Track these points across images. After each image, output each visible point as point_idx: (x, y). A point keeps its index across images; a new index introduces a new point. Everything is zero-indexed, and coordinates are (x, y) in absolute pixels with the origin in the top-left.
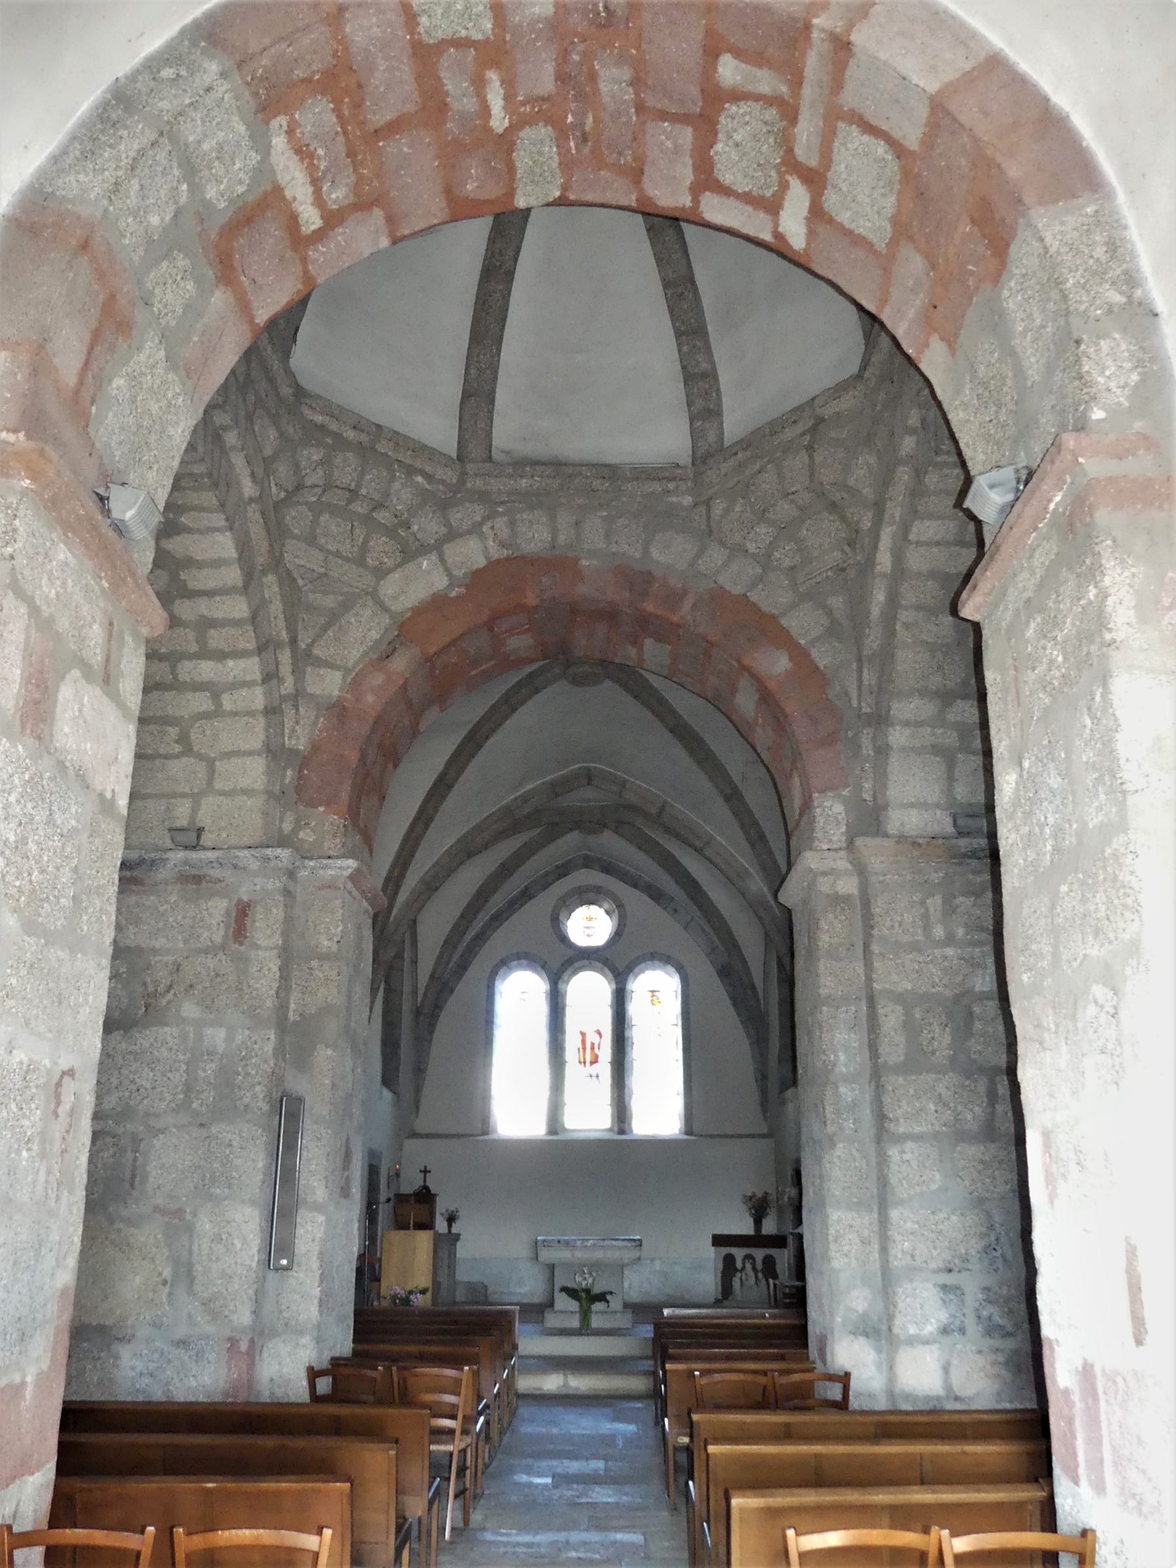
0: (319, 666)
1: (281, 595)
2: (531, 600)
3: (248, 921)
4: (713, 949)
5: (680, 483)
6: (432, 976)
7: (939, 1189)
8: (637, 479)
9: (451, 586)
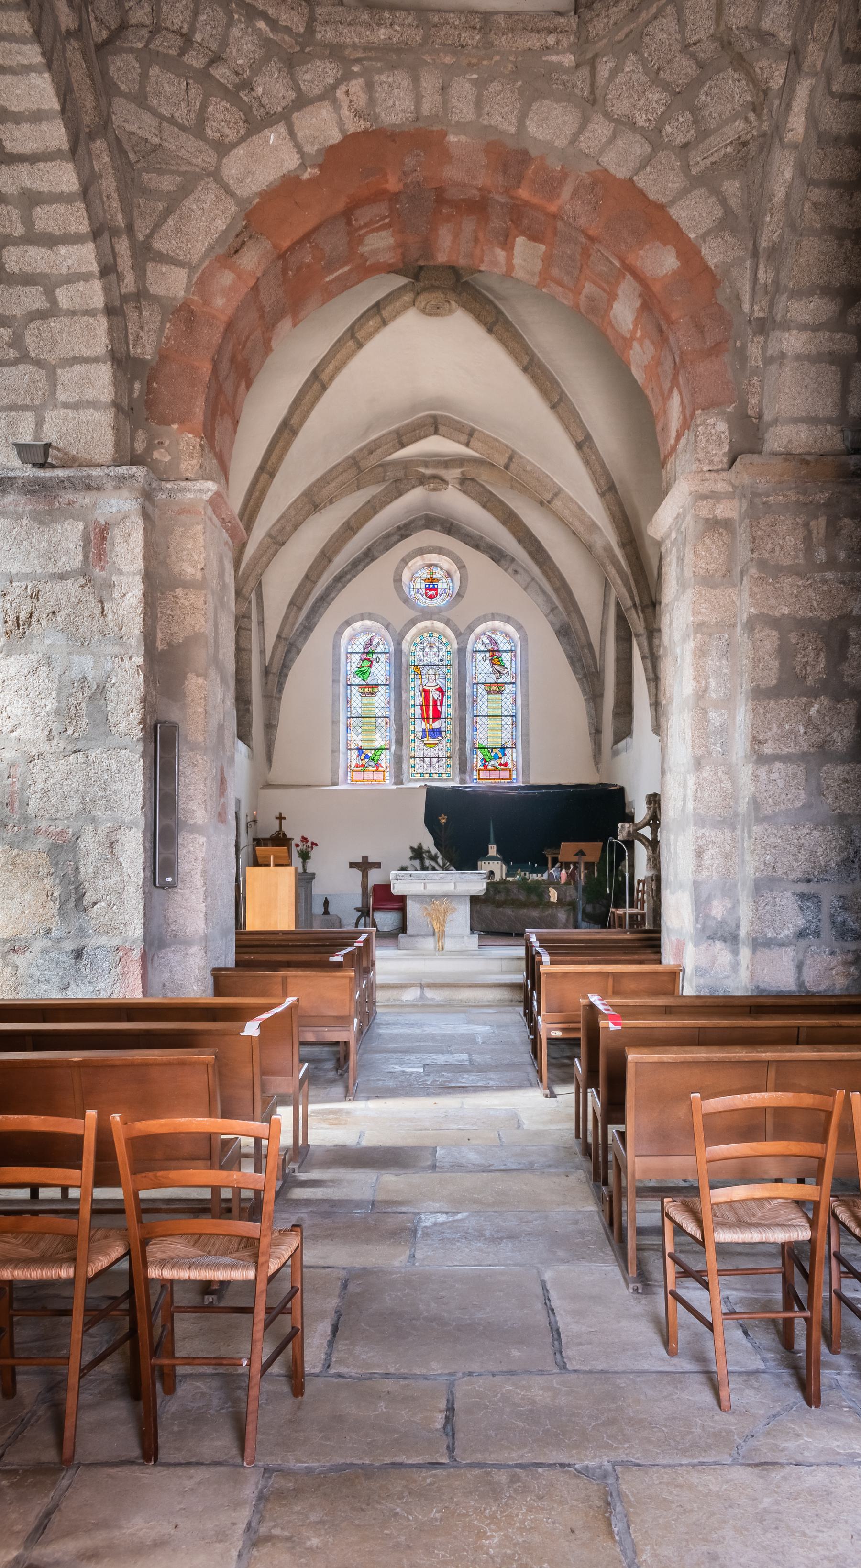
0: (161, 262)
1: (114, 168)
2: (393, 184)
3: (107, 546)
4: (552, 610)
5: (560, 36)
6: (279, 637)
7: (803, 806)
8: (512, 30)
9: (303, 166)
